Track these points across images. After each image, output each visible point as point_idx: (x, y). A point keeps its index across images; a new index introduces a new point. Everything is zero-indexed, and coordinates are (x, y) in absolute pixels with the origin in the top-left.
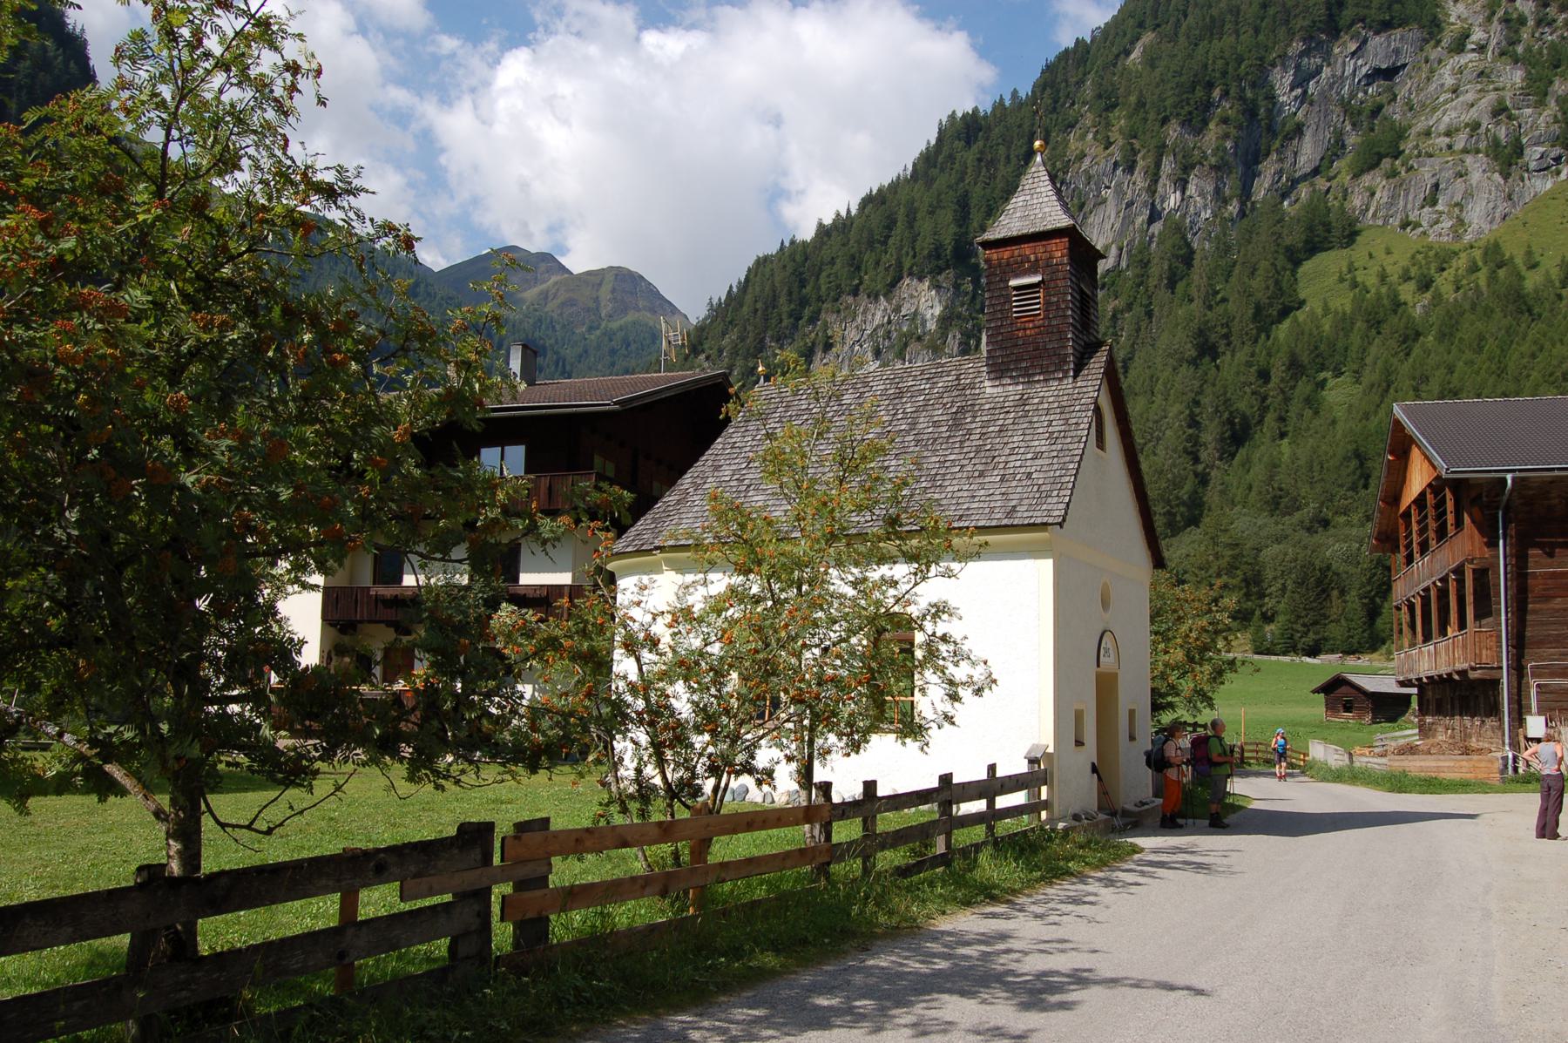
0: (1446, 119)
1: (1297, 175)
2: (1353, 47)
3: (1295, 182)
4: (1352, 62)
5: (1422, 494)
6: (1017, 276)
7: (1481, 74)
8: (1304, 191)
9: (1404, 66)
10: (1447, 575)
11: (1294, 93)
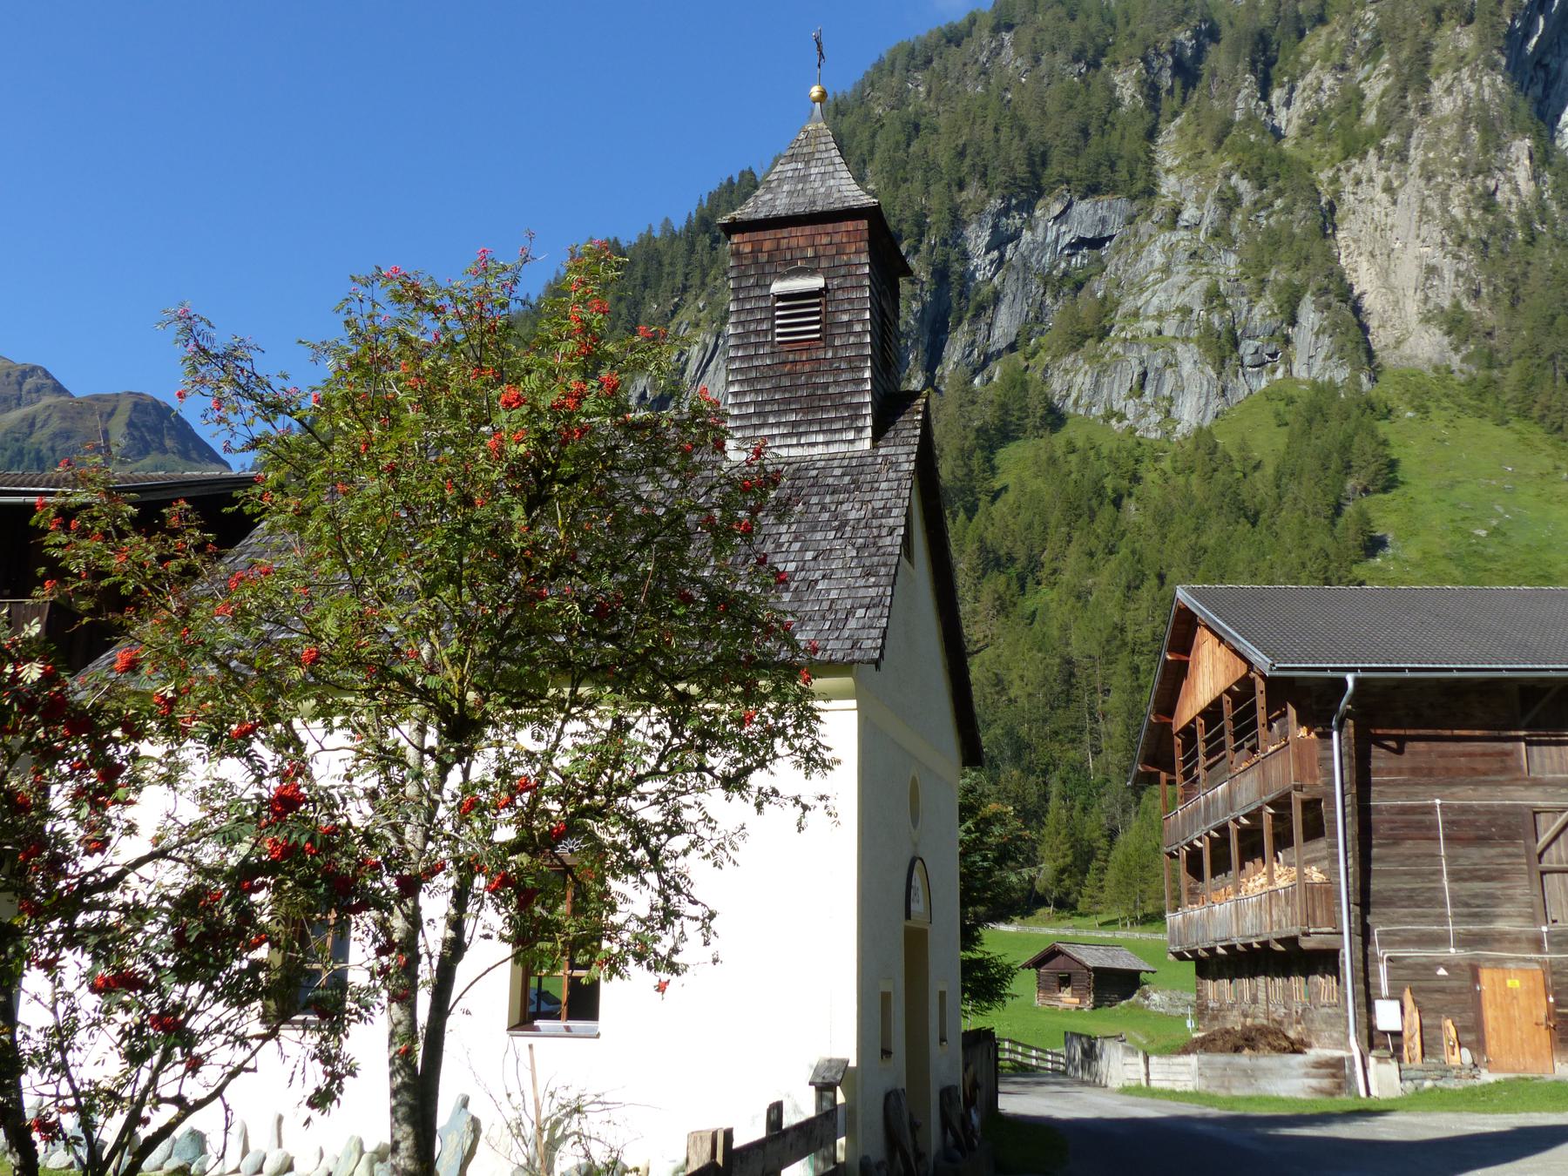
0: (1155, 301)
1: (992, 349)
2: (1057, 208)
3: (988, 358)
4: (1055, 227)
5: (1216, 704)
6: (783, 277)
7: (1193, 255)
8: (997, 370)
9: (1111, 238)
10: (1260, 809)
11: (990, 257)
